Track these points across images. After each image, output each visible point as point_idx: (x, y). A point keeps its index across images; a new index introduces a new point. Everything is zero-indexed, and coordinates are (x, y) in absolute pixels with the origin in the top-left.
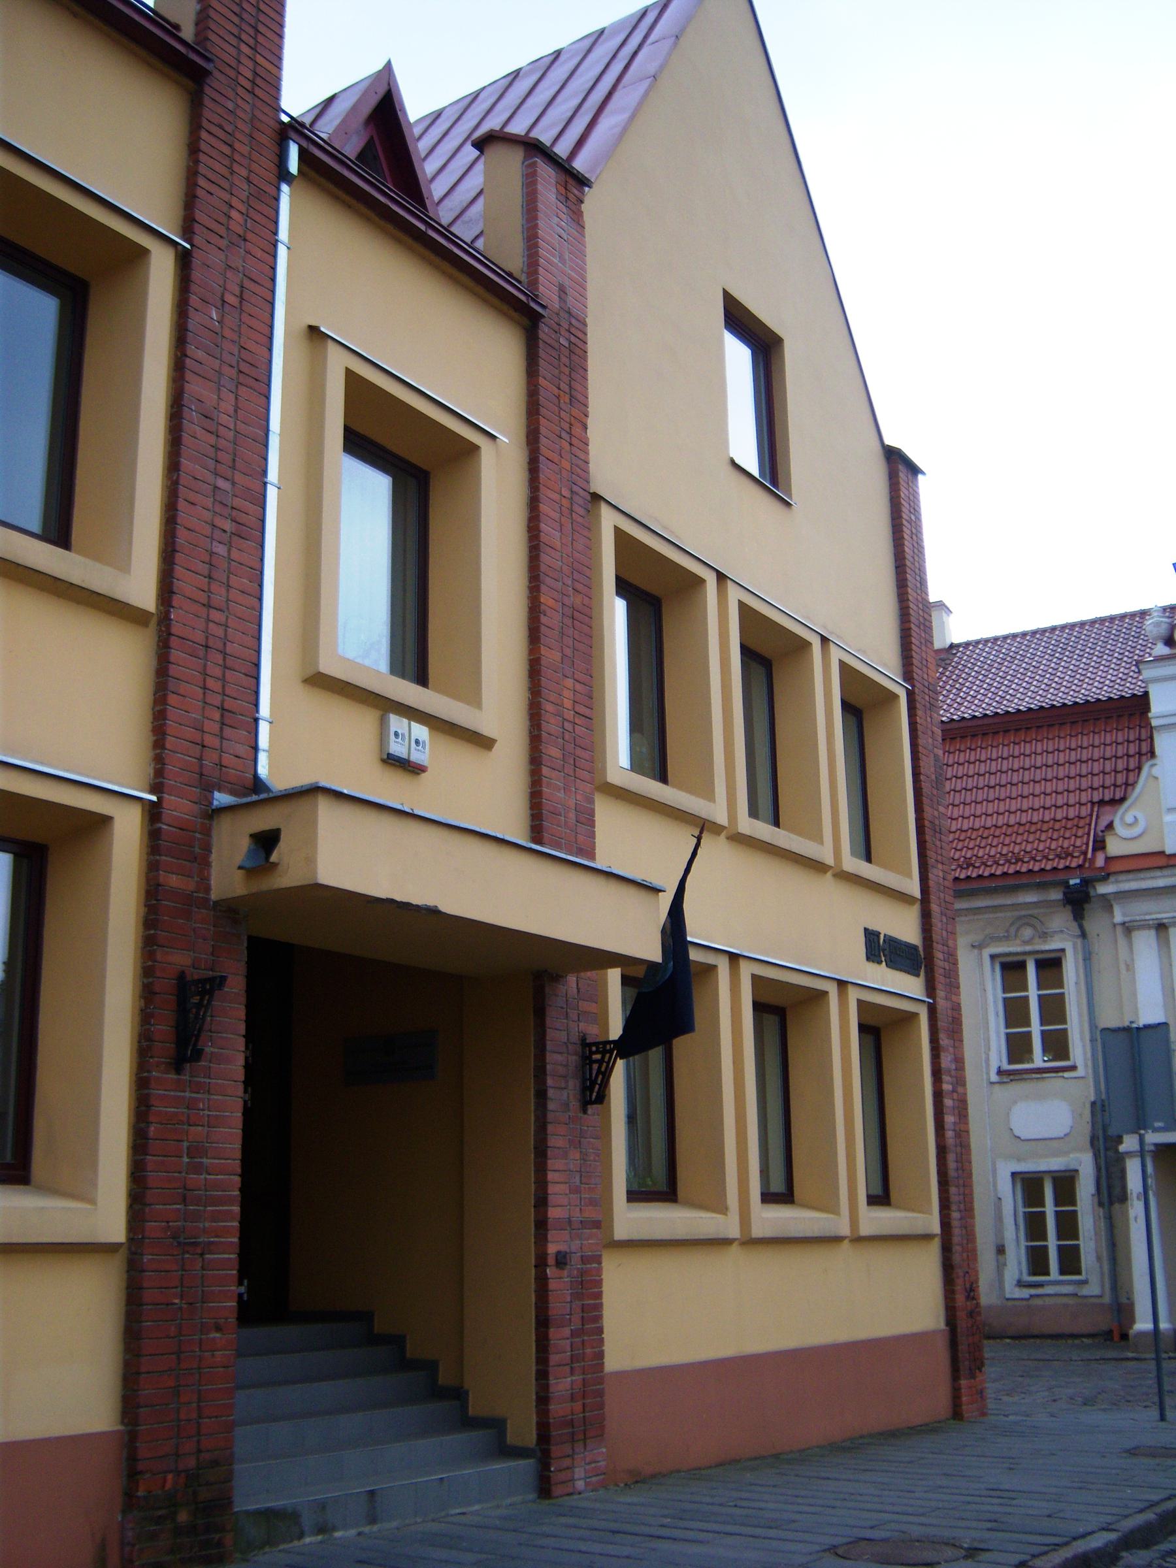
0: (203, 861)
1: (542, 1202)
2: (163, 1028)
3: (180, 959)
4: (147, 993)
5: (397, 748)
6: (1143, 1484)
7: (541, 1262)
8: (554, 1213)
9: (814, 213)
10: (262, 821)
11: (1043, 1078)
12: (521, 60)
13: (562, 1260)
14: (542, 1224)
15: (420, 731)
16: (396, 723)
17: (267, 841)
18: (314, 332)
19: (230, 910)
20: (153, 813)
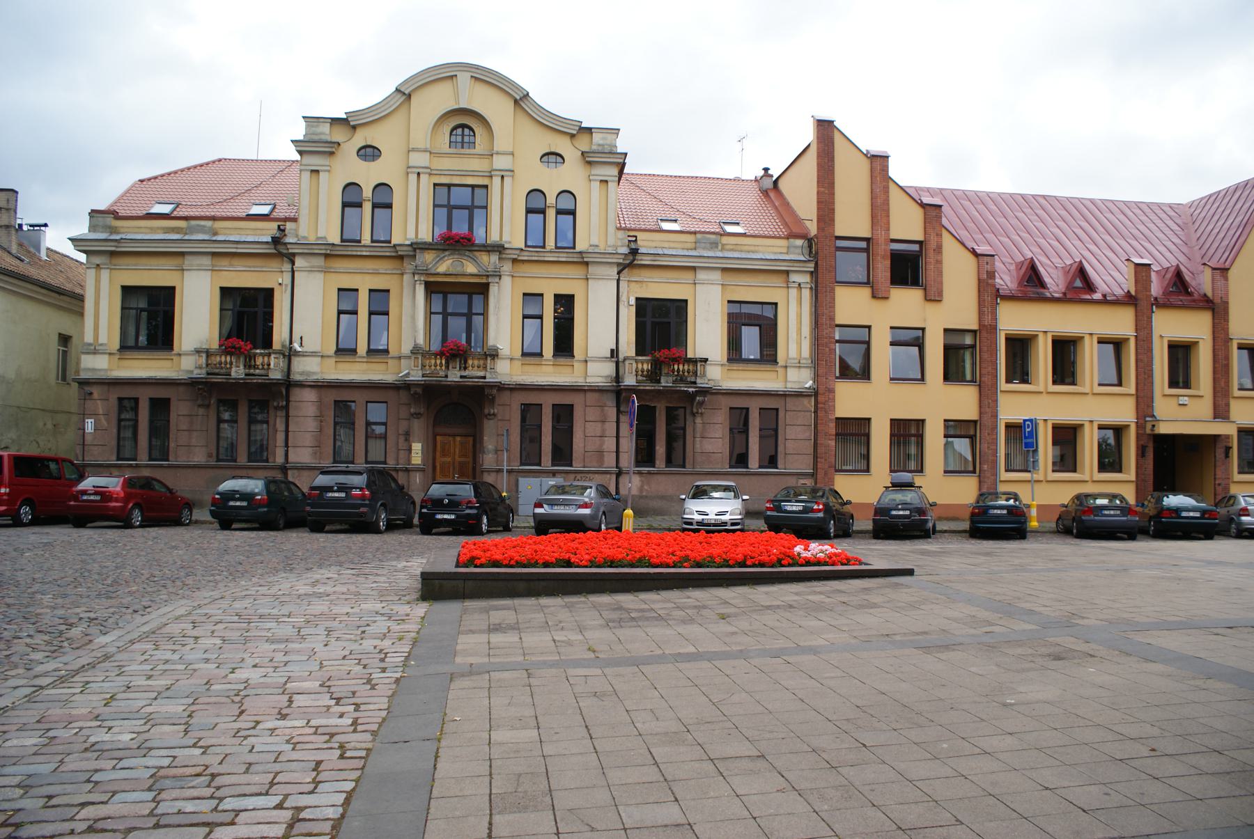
0: (1145, 428)
1: (1215, 475)
2: (1140, 452)
3: (1142, 442)
4: (1137, 448)
5: (1181, 403)
6: (732, 817)
7: (1215, 484)
8: (1217, 477)
9: (851, 141)
10: (1153, 423)
11: (897, 584)
12: (1204, 195)
13: (1219, 484)
14: (1215, 478)
15: (1186, 398)
16: (1181, 398)
17: (1154, 426)
18: (1161, 336)
19: (1149, 435)
20: (1137, 423)
